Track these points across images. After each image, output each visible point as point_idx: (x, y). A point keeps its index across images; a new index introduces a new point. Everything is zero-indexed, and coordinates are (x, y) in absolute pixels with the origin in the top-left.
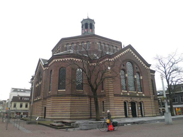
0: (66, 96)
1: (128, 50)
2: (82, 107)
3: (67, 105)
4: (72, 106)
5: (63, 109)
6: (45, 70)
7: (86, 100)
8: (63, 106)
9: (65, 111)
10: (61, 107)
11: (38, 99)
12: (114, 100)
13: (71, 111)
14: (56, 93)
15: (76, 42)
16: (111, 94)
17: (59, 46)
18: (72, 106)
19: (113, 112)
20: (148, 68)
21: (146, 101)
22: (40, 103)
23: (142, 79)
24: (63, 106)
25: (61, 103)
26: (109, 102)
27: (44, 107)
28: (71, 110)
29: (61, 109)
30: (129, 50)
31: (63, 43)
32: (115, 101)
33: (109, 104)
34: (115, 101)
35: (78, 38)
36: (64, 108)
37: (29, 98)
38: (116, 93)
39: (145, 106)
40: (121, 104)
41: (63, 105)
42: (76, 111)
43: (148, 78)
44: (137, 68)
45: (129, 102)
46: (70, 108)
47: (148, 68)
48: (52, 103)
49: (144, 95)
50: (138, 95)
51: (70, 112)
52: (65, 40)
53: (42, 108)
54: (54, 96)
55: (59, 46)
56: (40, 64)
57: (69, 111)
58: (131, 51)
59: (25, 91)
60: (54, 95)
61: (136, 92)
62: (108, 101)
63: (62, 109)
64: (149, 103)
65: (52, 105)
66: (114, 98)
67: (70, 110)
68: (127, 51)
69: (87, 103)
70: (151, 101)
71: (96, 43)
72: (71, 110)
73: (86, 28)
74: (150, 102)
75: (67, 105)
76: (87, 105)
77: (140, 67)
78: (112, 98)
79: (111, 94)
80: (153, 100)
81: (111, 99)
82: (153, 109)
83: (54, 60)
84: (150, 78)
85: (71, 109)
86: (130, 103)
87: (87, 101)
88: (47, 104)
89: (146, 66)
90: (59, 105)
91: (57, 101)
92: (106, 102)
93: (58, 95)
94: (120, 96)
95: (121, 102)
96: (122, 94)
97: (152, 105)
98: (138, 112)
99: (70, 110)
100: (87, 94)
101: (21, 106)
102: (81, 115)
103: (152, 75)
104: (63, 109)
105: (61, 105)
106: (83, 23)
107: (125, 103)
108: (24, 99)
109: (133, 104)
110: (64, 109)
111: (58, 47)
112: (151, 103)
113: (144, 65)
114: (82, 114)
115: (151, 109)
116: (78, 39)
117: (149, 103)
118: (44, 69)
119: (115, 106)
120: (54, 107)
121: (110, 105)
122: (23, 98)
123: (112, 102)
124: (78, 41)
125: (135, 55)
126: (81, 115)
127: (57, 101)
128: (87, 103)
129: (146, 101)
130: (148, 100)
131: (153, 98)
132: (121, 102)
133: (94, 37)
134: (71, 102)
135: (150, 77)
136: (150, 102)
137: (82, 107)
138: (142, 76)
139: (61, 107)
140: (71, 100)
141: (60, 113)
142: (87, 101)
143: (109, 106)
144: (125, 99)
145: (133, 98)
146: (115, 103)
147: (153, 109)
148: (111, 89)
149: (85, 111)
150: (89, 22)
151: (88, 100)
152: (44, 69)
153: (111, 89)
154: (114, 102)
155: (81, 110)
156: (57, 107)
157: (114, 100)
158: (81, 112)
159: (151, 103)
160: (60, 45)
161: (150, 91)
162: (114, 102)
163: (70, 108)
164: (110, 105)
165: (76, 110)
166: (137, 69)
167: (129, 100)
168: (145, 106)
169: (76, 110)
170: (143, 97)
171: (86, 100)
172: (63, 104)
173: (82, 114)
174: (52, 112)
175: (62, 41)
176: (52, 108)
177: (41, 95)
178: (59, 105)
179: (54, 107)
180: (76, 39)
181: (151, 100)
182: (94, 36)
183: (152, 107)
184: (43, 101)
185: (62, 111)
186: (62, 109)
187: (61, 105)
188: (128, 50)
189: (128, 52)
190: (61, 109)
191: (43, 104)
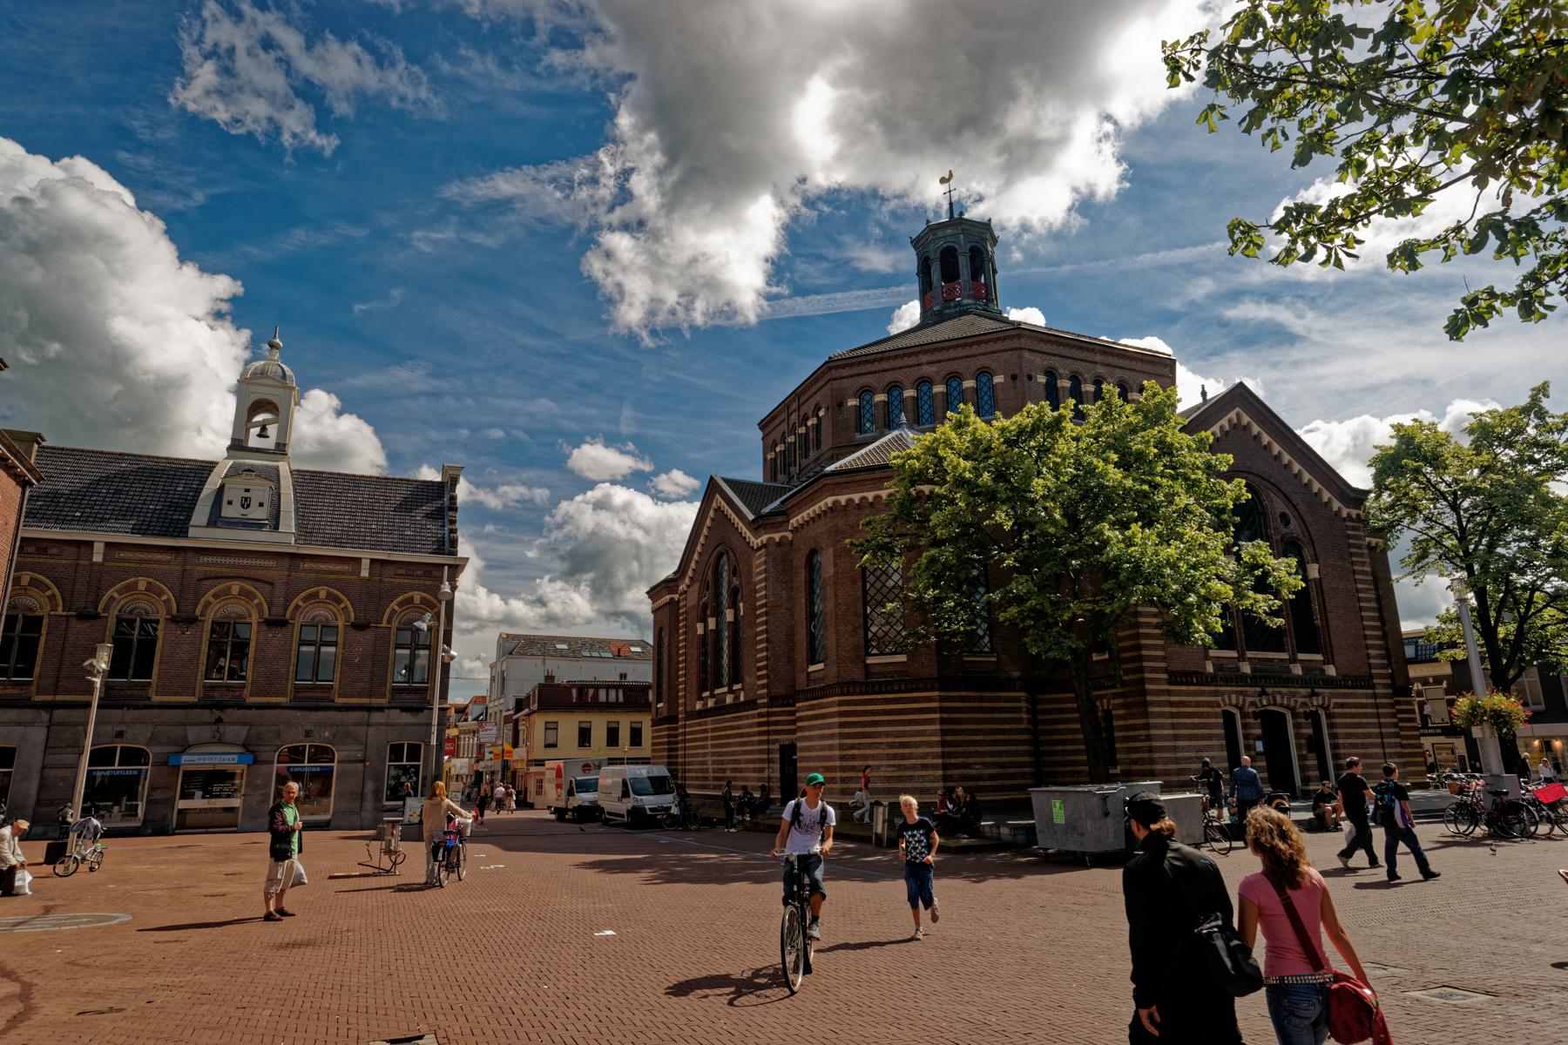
0: (896, 687)
1: (1230, 420)
2: (997, 743)
3: (922, 733)
4: (948, 738)
5: (903, 757)
6: (764, 546)
7: (1017, 705)
8: (898, 740)
9: (913, 767)
10: (891, 745)
11: (711, 703)
12: (1171, 704)
13: (945, 767)
14: (857, 674)
15: (915, 373)
16: (1154, 670)
17: (813, 402)
18: (948, 738)
19: (1169, 767)
20: (1349, 515)
21: (1348, 706)
22: (751, 726)
23: (1320, 579)
24: (898, 740)
25: (889, 723)
26: (1147, 715)
27: (777, 746)
28: (947, 761)
29: (888, 757)
30: (1238, 415)
31: (836, 384)
32: (1174, 710)
33: (1147, 727)
34: (1174, 710)
35: (926, 352)
36: (907, 751)
37: (621, 693)
38: (1178, 666)
39: (1339, 731)
40: (1205, 726)
41: (899, 734)
42: (968, 766)
43: (1354, 572)
44: (1283, 516)
45: (1251, 710)
46: (938, 750)
47: (1349, 515)
48: (842, 725)
49: (1331, 671)
50: (1297, 670)
51: (940, 772)
52: (851, 365)
53: (769, 751)
54: (844, 687)
55: (813, 402)
56: (718, 510)
57: (935, 767)
58: (1246, 419)
59: (619, 651)
60: (848, 684)
61: (1285, 656)
62: (1138, 702)
63: (895, 757)
64: (1366, 715)
65: (842, 736)
66: (1169, 693)
67: (939, 761)
68: (1224, 422)
69: (1020, 721)
70: (1377, 706)
71: (1030, 378)
72: (947, 761)
73: (950, 275)
74: (1369, 711)
75: (922, 733)
76: (1021, 732)
77: (1302, 508)
78: (1161, 692)
79: (1154, 670)
80: (1385, 696)
81: (1155, 698)
82: (1387, 751)
83: (830, 500)
84: (1368, 569)
85: (943, 755)
86: (1256, 715)
87: (1019, 710)
88: (802, 729)
89: (1336, 505)
90: (879, 735)
91: (866, 713)
92: (1121, 717)
93: (867, 684)
94: (1202, 678)
95: (1208, 715)
96: (1210, 668)
97: (1380, 725)
98: (1303, 768)
99: (939, 761)
100: (1016, 674)
101: (584, 737)
102: (994, 783)
103: (1371, 548)
104: (903, 757)
105: (887, 735)
106: (934, 250)
107: (1228, 718)
108: (596, 695)
109: (1272, 724)
110: (910, 756)
111: (808, 408)
112: (1378, 716)
113: (1325, 499)
114: (999, 783)
115: (1379, 750)
116: (924, 359)
117: (1366, 715)
118: (756, 542)
119: (1176, 737)
120: (853, 747)
121: (1152, 732)
122: (591, 691)
123: (1161, 715)
124: (927, 370)
125: (1249, 423)
126: (994, 783)
127: (866, 713)
128: (1020, 721)
129: (1348, 706)
130: (1361, 696)
131: (1385, 686)
132: (1208, 715)
133: (1015, 343)
134: (942, 721)
135: (1363, 564)
136: (1369, 711)
137: (997, 743)
138: (1316, 560)
139: (891, 745)
140: (942, 710)
141: (889, 779)
142: (1019, 710)
143: (1148, 738)
144: (1230, 698)
145: (1269, 690)
146: (1175, 721)
147: (1387, 751)
148: (1156, 647)
149: (1015, 765)
150: (963, 245)
151: (1023, 704)
152: (756, 542)
153: (1156, 647)
154: (1172, 715)
155: (994, 759)
156: (871, 746)
157: (1171, 704)
158: (994, 771)
159: (1380, 725)
160: (817, 398)
161: (1367, 647)
162: (1172, 715)
163: (938, 750)
164: (1152, 732)
165: (972, 760)
166: (1287, 523)
167: (1253, 704)
168: (1339, 731)
169: (972, 760)
170: (1330, 682)
171: (1017, 705)
172: (901, 728)
173: (999, 783)
174: (843, 769)
175: (834, 374)
176: (844, 753)
177: (748, 679)
178: (879, 735)
179: (853, 747)
180: (912, 360)
181: (1375, 696)
182: (1019, 336)
183: (1381, 736)
184: (768, 714)
185: (900, 767)
186: (895, 757)
187: (887, 735)
188: (1232, 415)
189: (1234, 427)
190: (888, 757)
191: (771, 728)
